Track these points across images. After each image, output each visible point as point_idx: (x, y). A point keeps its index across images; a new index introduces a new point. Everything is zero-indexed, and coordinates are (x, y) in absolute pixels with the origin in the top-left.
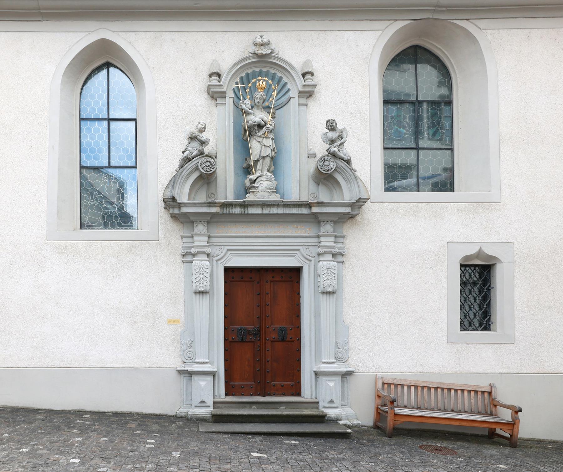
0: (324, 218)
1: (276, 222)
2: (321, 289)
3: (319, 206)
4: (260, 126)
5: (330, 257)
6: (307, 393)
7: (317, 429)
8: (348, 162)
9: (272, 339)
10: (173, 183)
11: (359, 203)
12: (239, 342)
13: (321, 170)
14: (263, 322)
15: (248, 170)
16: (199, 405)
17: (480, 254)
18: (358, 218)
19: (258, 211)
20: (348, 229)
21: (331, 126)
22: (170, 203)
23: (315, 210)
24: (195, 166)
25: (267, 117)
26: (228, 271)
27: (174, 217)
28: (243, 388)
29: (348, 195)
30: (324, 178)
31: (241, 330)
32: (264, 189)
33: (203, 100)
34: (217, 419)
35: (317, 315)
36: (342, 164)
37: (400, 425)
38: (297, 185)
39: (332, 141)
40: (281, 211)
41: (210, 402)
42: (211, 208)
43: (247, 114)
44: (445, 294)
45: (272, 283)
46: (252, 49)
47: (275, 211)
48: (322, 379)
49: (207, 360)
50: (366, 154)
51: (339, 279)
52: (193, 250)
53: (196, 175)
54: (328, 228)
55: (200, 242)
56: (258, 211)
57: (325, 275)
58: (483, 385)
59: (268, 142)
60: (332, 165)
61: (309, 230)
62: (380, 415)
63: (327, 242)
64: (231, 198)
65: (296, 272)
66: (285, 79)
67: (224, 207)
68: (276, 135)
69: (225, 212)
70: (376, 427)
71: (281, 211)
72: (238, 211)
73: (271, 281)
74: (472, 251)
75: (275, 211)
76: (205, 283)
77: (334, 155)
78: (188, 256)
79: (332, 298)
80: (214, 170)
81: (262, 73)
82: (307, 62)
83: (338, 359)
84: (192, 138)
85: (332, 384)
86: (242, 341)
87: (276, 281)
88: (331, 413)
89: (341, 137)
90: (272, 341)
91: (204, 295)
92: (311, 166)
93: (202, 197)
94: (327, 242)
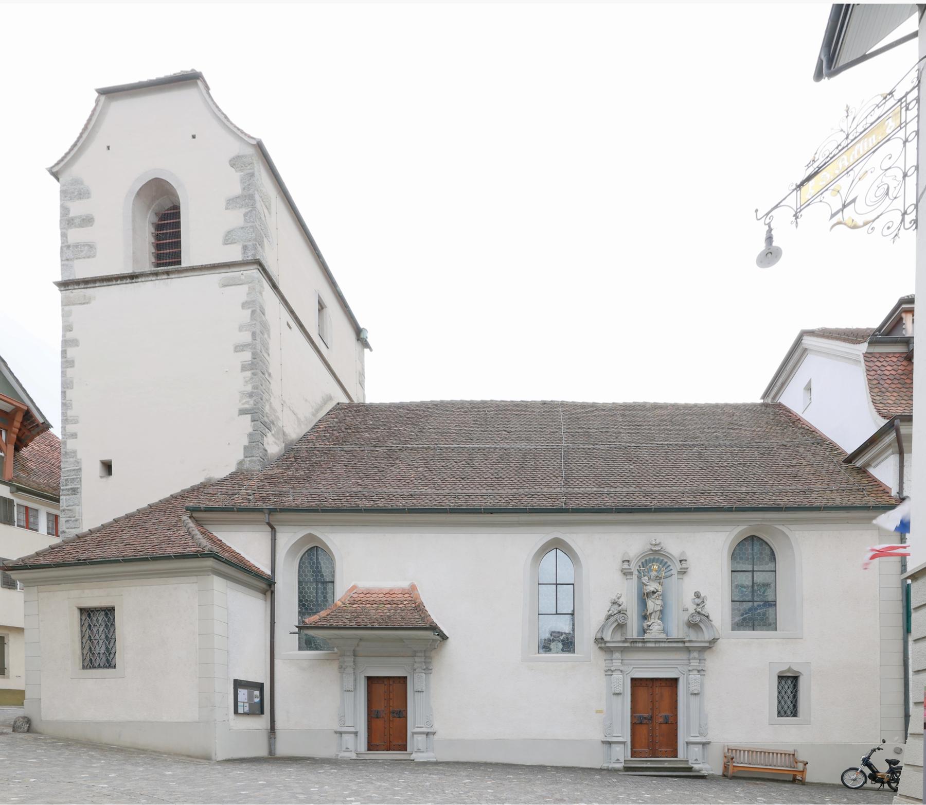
2: (691, 691)
4: (654, 592)
5: (696, 672)
6: (681, 754)
7: (688, 774)
8: (707, 617)
10: (602, 629)
11: (714, 641)
12: (573, 620)
14: (654, 714)
15: (645, 617)
17: (789, 670)
19: (653, 645)
20: (707, 655)
21: (697, 595)
22: (599, 641)
23: (687, 644)
25: (659, 588)
26: (632, 679)
27: (600, 648)
29: (707, 636)
30: (693, 625)
31: (640, 717)
32: (656, 631)
33: (618, 576)
34: (627, 769)
35: (688, 707)
36: (703, 618)
37: (735, 773)
38: (677, 630)
39: (698, 605)
40: (666, 645)
41: (622, 760)
43: (646, 585)
44: (767, 694)
46: (649, 547)
47: (663, 645)
48: (691, 746)
50: (720, 610)
51: (702, 685)
52: (613, 669)
53: (616, 624)
54: (695, 655)
55: (617, 664)
56: (653, 645)
58: (790, 750)
59: (659, 602)
60: (698, 619)
61: (684, 656)
62: (726, 767)
63: (694, 663)
64: (635, 636)
65: (675, 681)
66: (669, 563)
68: (663, 597)
70: (724, 775)
71: (666, 645)
72: (640, 645)
74: (785, 668)
75: (663, 645)
77: (699, 613)
78: (609, 672)
79: (697, 698)
81: (655, 560)
82: (683, 553)
83: (701, 734)
84: (614, 603)
85: (697, 749)
88: (696, 767)
89: (703, 602)
92: (686, 617)
93: (618, 637)
94: (694, 663)
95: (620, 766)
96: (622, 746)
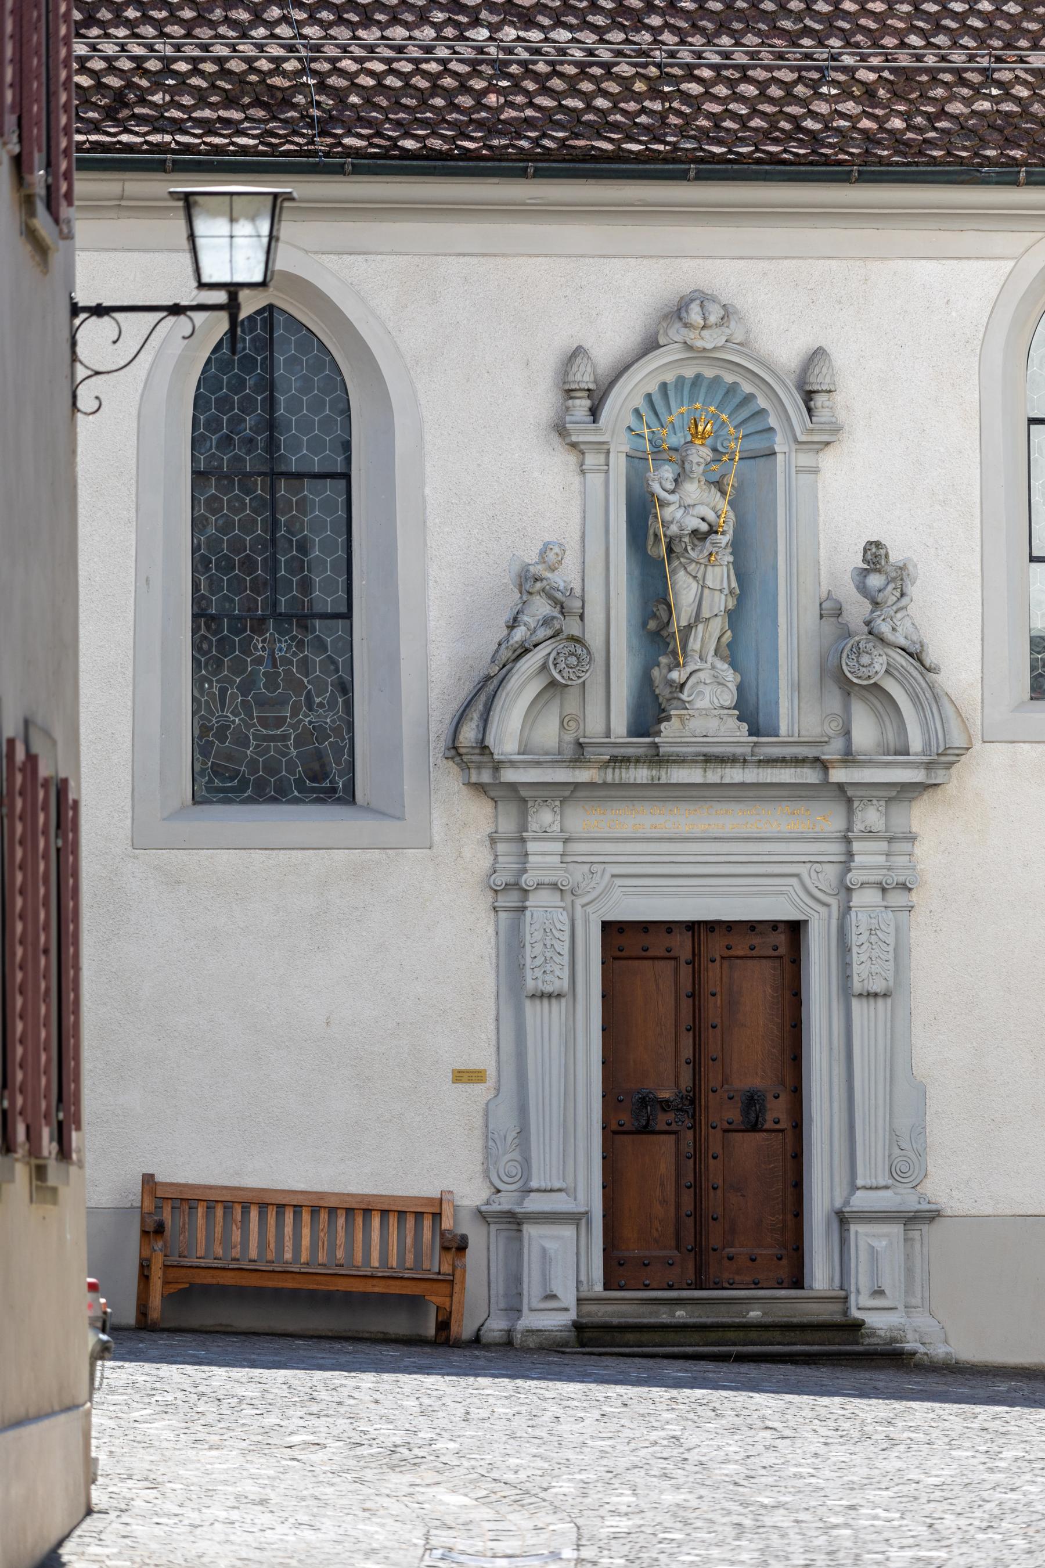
0: (859, 793)
1: (737, 799)
3: (477, 676)
6: (820, 1275)
9: (726, 1126)
11: (943, 758)
13: (844, 667)
16: (543, 1305)
18: (951, 789)
20: (921, 817)
24: (540, 663)
26: (606, 925)
28: (648, 1265)
41: (569, 1298)
42: (577, 772)
45: (726, 963)
47: (735, 775)
49: (557, 1185)
57: (864, 947)
67: (607, 767)
69: (609, 779)
71: (750, 775)
73: (723, 958)
76: (558, 973)
80: (569, 683)
86: (646, 1130)
87: (738, 957)
90: (725, 1131)
91: (554, 1001)
93: (548, 733)
95: (555, 1321)
96: (568, 1232)
